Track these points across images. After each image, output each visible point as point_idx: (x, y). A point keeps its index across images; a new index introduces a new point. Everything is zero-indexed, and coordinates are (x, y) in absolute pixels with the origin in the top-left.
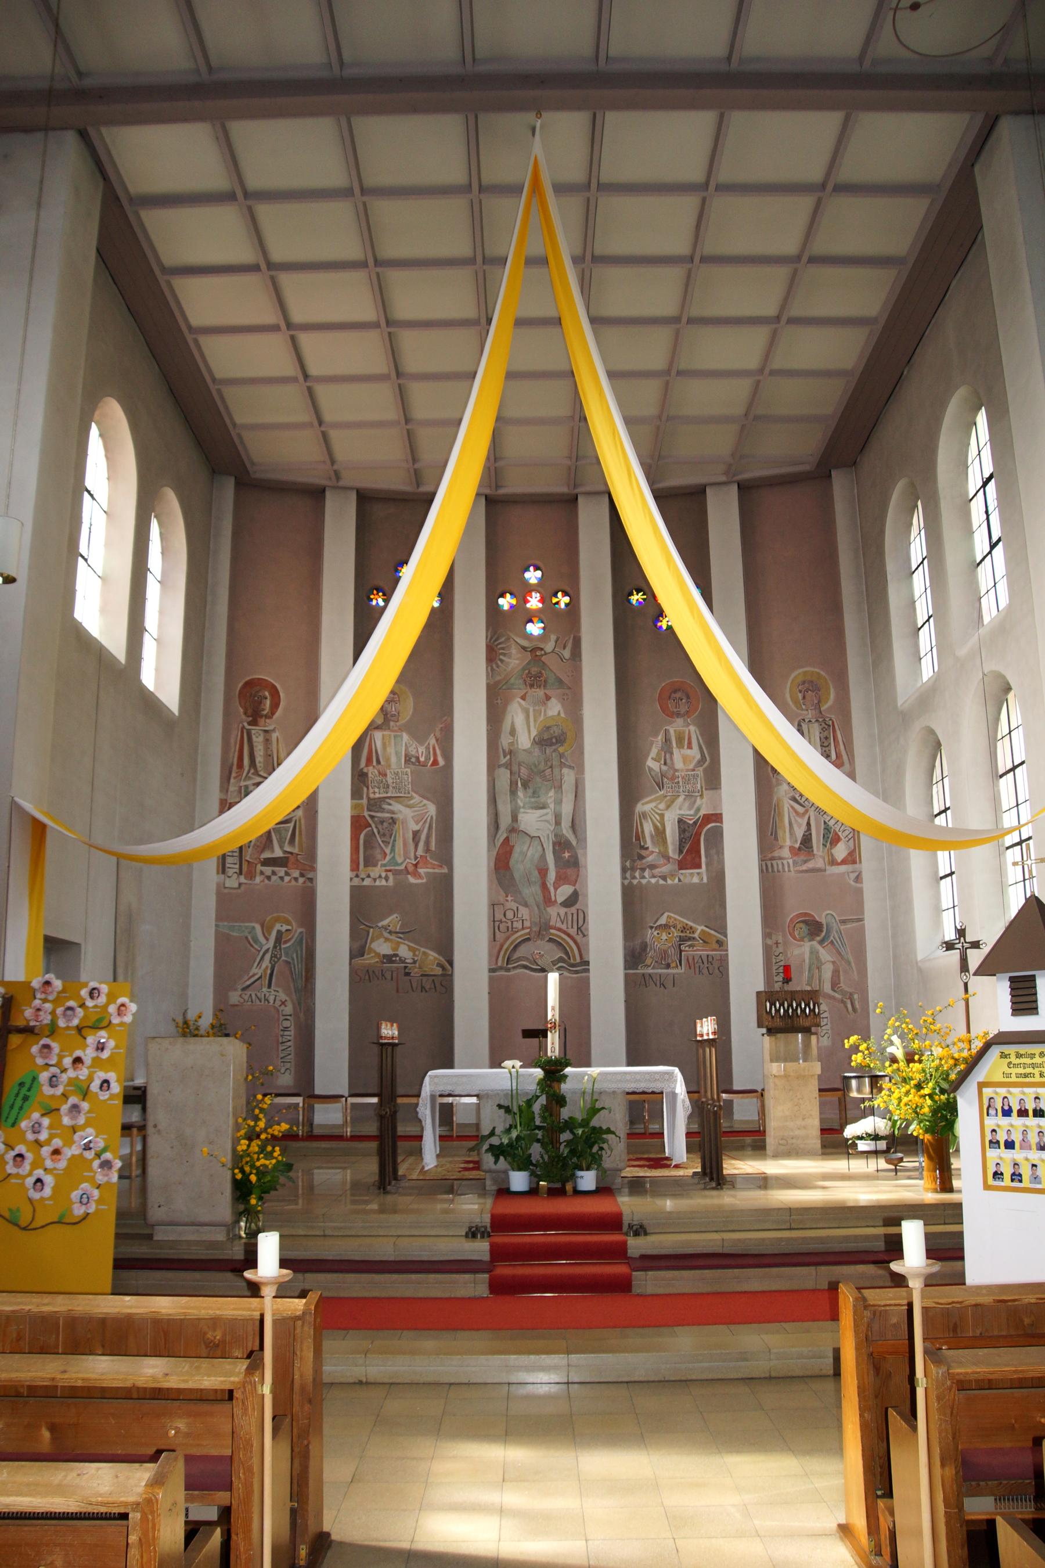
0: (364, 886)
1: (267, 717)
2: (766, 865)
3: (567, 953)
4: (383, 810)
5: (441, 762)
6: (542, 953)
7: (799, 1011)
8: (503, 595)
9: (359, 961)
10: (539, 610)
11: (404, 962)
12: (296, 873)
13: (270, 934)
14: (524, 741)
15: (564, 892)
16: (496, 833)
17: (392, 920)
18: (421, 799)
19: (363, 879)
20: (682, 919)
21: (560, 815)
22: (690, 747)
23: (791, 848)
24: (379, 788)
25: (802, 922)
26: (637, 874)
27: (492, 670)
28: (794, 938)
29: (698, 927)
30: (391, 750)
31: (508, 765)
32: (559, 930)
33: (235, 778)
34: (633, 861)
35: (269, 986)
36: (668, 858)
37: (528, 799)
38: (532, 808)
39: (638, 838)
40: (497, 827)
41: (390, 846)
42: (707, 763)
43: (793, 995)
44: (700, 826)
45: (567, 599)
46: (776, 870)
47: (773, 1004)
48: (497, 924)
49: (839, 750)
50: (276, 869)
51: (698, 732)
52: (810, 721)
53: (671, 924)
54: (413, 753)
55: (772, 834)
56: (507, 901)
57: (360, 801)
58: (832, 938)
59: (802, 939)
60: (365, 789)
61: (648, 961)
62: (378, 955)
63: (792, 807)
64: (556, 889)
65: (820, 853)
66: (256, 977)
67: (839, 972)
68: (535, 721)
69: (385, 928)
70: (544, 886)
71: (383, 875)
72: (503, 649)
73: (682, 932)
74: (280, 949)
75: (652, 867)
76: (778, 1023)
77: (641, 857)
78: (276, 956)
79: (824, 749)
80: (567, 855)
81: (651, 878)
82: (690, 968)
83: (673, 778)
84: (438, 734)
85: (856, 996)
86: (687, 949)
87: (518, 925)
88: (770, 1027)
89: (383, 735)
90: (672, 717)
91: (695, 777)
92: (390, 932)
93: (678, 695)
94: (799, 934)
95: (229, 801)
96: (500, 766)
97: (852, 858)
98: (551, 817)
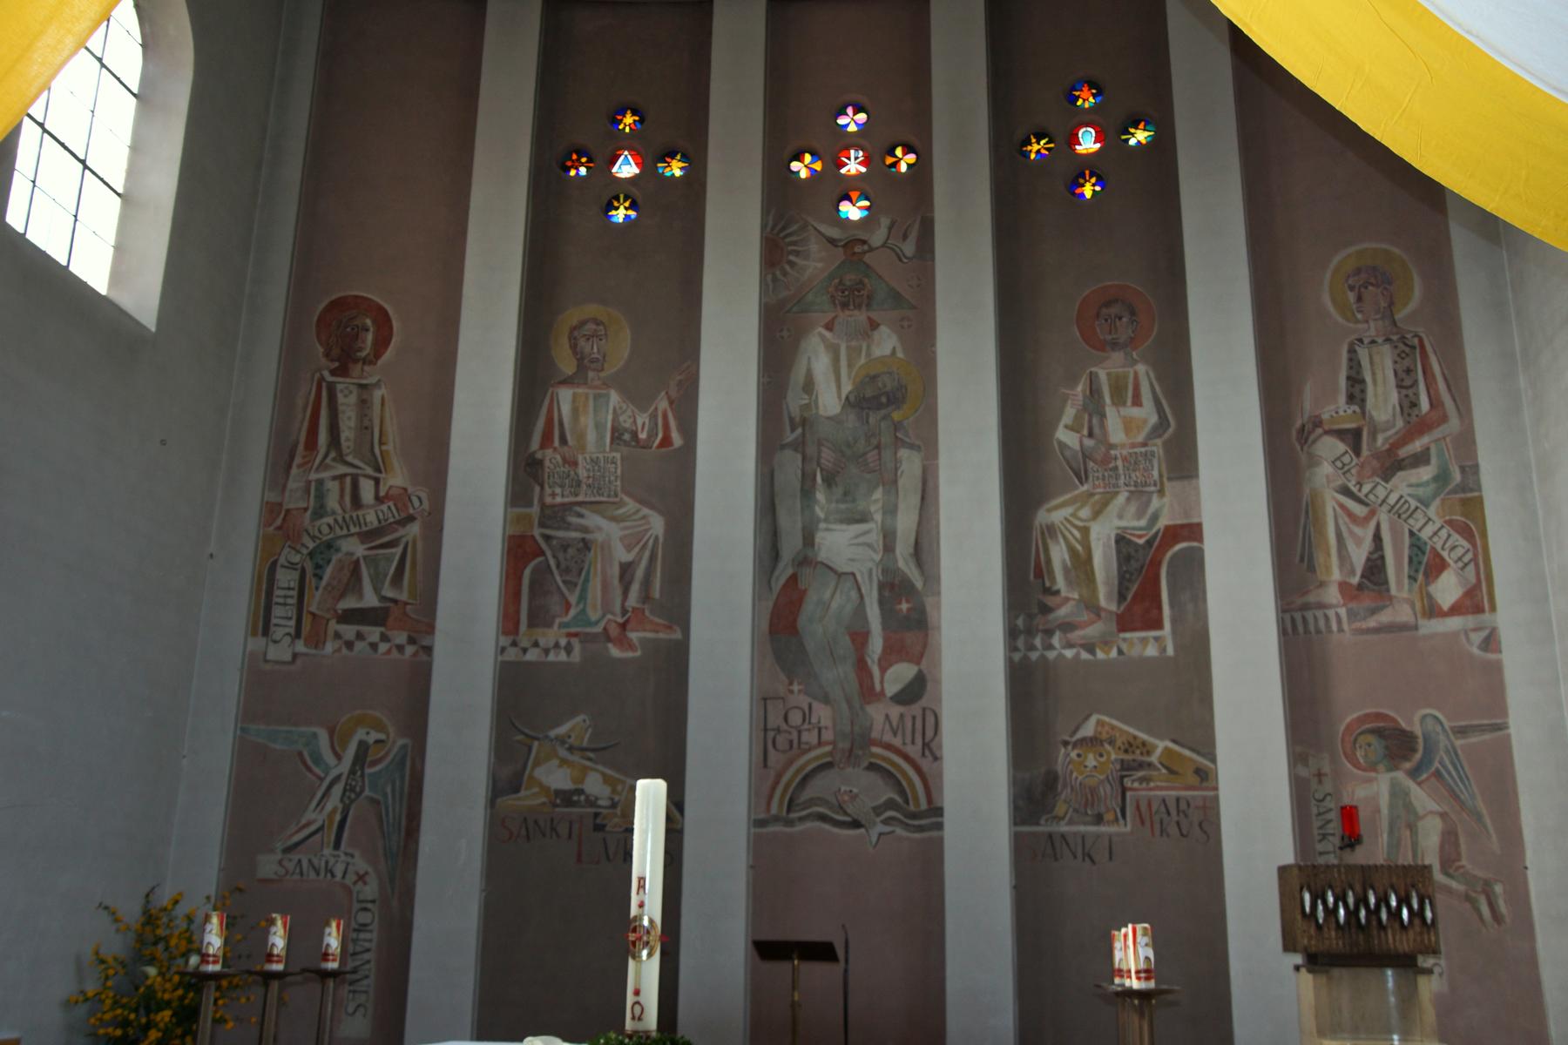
0: (529, 663)
1: (365, 361)
2: (1293, 621)
3: (902, 792)
4: (568, 527)
5: (677, 440)
6: (855, 790)
7: (1384, 916)
8: (798, 157)
9: (507, 802)
10: (860, 175)
11: (592, 802)
12: (401, 638)
13: (344, 748)
14: (829, 401)
15: (901, 673)
16: (772, 572)
17: (574, 726)
18: (638, 505)
19: (525, 650)
20: (1125, 727)
21: (894, 533)
22: (1137, 402)
23: (1343, 587)
24: (562, 486)
25: (1373, 731)
26: (1038, 642)
27: (775, 280)
28: (1356, 765)
29: (1157, 742)
30: (588, 421)
31: (799, 445)
32: (888, 747)
33: (299, 466)
34: (1030, 617)
35: (337, 846)
36: (1096, 611)
37: (833, 505)
38: (842, 521)
39: (1039, 574)
40: (775, 555)
41: (579, 588)
42: (1171, 430)
43: (1367, 876)
44: (1160, 546)
45: (911, 158)
46: (1312, 628)
47: (1318, 896)
48: (771, 734)
49: (1437, 390)
50: (365, 629)
51: (1152, 375)
52: (1373, 342)
53: (1104, 736)
54: (627, 425)
55: (1302, 560)
56: (792, 692)
57: (528, 510)
58: (1436, 764)
59: (1373, 767)
60: (537, 489)
61: (1060, 809)
62: (545, 789)
63: (1342, 506)
64: (883, 670)
65: (1405, 595)
66: (313, 828)
67: (1456, 835)
68: (850, 366)
69: (562, 740)
70: (861, 666)
71: (563, 642)
72: (794, 243)
73: (1126, 751)
74: (362, 776)
75: (1067, 627)
76: (1333, 941)
77: (1046, 610)
78: (352, 790)
79: (1404, 392)
80: (904, 606)
81: (1064, 647)
82: (1143, 822)
83: (1106, 460)
84: (673, 394)
85: (1498, 889)
86: (1136, 785)
87: (810, 737)
88: (1313, 950)
89: (575, 395)
90: (1102, 349)
91: (1148, 456)
92: (571, 749)
93: (1114, 310)
94: (1366, 756)
95: (285, 507)
96: (783, 447)
97: (1476, 601)
98: (875, 538)
